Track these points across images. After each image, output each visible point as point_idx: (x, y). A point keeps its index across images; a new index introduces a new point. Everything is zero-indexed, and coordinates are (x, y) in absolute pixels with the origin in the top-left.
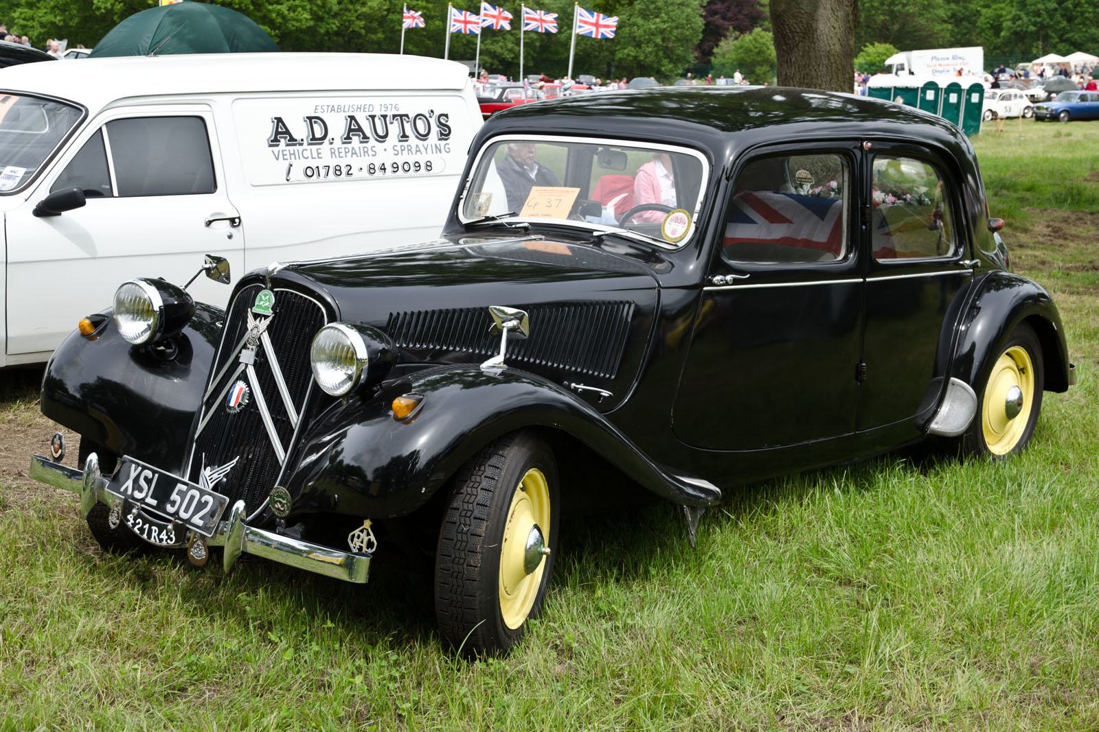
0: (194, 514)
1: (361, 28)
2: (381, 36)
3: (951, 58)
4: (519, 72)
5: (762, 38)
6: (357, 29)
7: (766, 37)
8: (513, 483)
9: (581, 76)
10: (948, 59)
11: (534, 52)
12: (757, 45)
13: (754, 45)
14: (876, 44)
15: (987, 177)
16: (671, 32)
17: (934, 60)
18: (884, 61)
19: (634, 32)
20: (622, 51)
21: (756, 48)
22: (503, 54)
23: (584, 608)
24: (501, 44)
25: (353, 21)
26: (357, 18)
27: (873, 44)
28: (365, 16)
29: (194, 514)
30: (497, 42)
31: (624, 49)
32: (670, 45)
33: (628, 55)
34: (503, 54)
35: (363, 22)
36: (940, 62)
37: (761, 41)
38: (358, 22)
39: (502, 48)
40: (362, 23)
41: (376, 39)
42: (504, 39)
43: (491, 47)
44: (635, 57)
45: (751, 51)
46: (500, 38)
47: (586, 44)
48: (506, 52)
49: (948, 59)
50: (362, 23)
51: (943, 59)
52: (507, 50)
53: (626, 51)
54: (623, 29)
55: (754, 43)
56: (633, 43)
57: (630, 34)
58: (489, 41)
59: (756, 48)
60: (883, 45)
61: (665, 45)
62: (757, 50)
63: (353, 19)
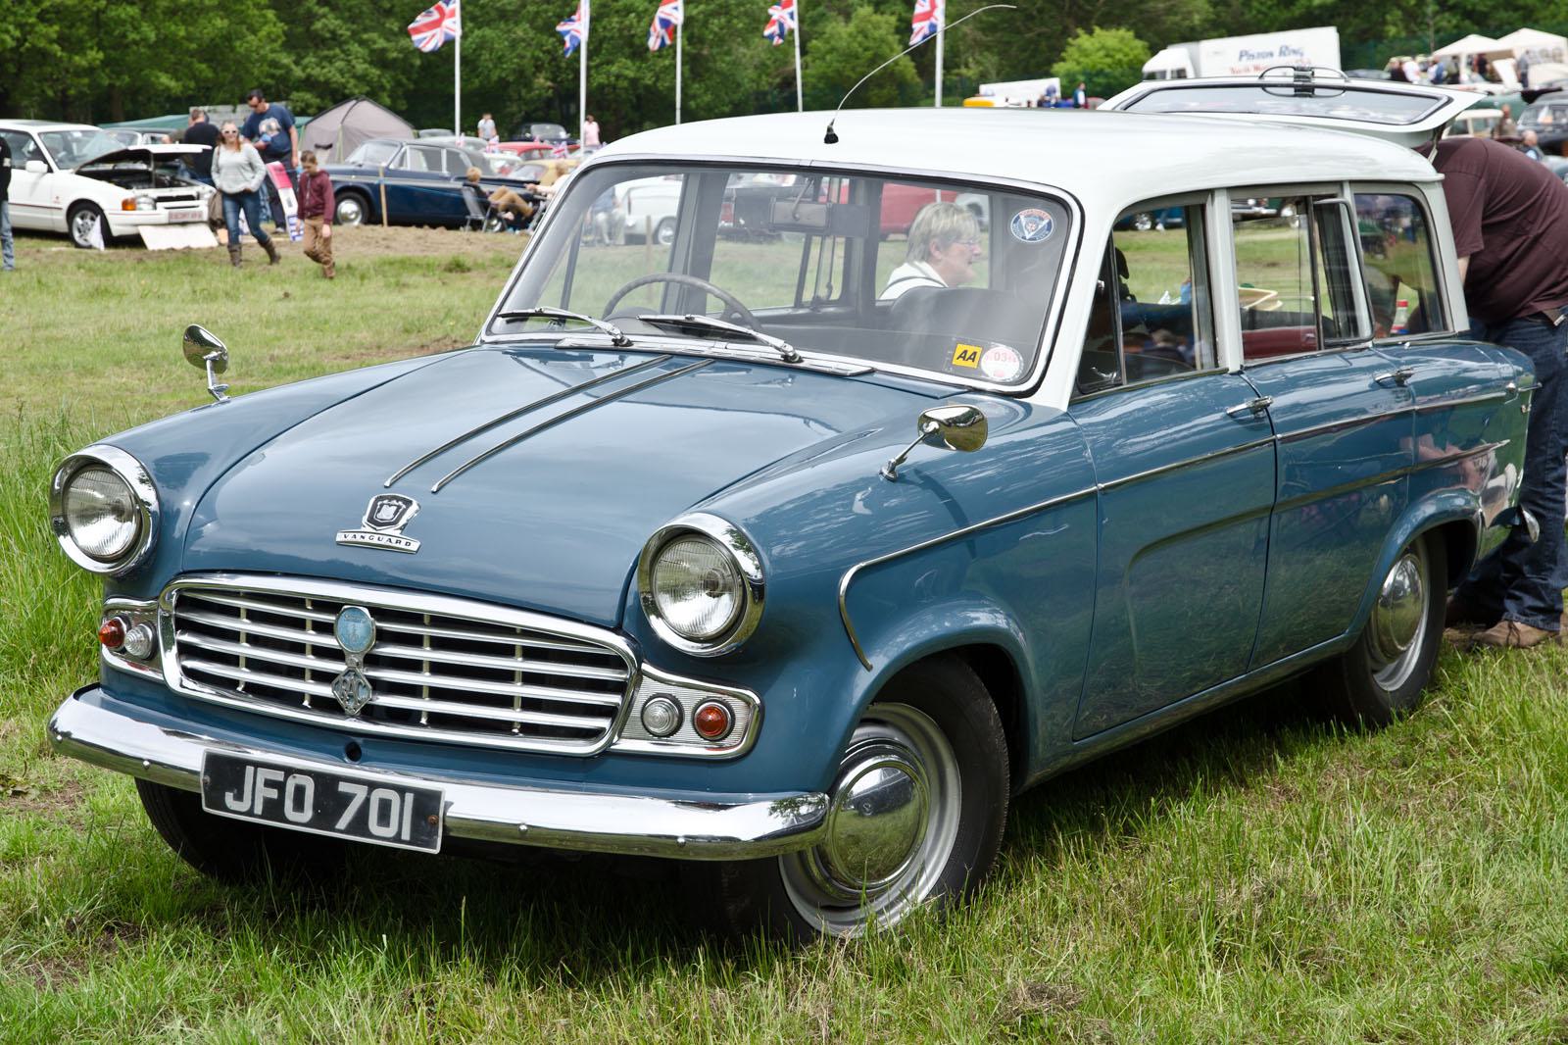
0: (367, 801)
1: (51, 41)
2: (95, 56)
3: (1276, 53)
4: (803, 96)
5: (877, 27)
6: (42, 44)
7: (884, 26)
8: (1118, 488)
9: (534, 127)
10: (1271, 54)
11: (409, 79)
12: (871, 44)
13: (860, 44)
14: (1097, 30)
15: (1419, 240)
16: (705, 24)
17: (1244, 58)
18: (1143, 63)
19: (631, 27)
20: (606, 68)
21: (866, 49)
22: (344, 87)
23: (857, 978)
24: (340, 64)
25: (33, 25)
26: (42, 17)
27: (1090, 32)
28: (58, 12)
29: (367, 801)
30: (330, 60)
31: (609, 62)
32: (705, 52)
33: (618, 77)
34: (344, 87)
35: (56, 28)
36: (1256, 62)
37: (877, 34)
38: (42, 28)
39: (341, 72)
40: (54, 30)
41: (84, 63)
42: (347, 53)
43: (316, 72)
44: (634, 82)
45: (857, 57)
46: (337, 51)
47: (522, 57)
48: (353, 82)
49: (1271, 54)
50: (54, 30)
51: (1261, 55)
52: (354, 76)
53: (614, 69)
54: (605, 22)
55: (860, 38)
56: (627, 50)
57: (620, 30)
58: (310, 59)
59: (866, 49)
60: (1113, 32)
61: (694, 51)
62: (869, 54)
63: (32, 20)
